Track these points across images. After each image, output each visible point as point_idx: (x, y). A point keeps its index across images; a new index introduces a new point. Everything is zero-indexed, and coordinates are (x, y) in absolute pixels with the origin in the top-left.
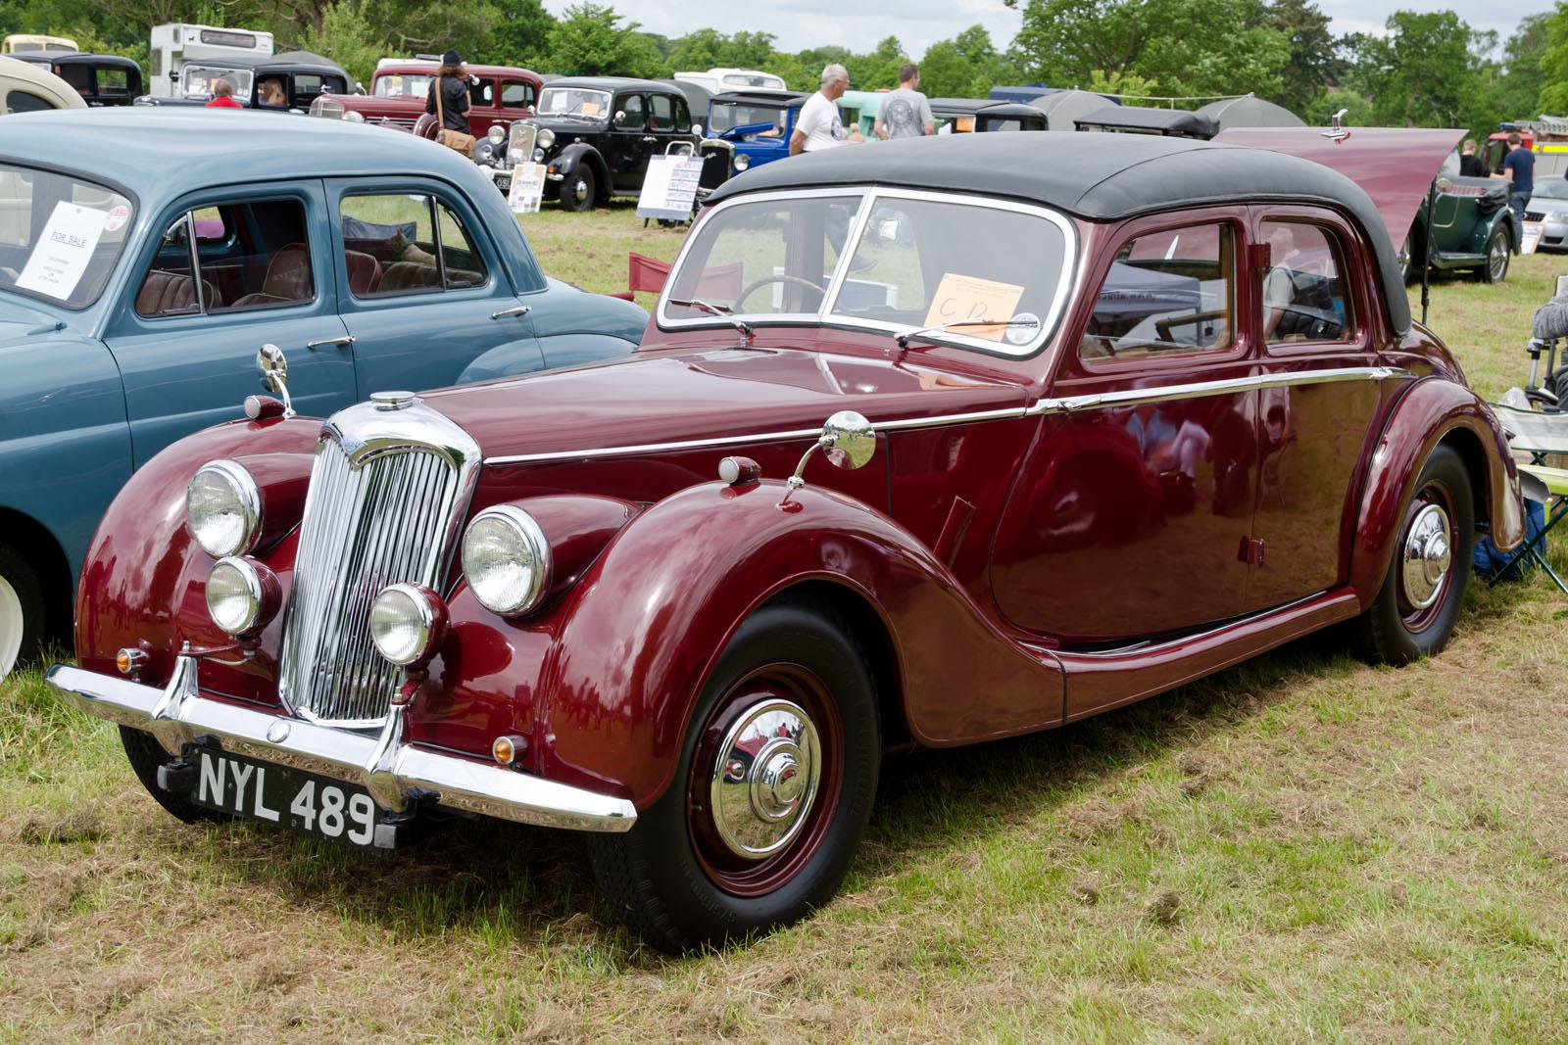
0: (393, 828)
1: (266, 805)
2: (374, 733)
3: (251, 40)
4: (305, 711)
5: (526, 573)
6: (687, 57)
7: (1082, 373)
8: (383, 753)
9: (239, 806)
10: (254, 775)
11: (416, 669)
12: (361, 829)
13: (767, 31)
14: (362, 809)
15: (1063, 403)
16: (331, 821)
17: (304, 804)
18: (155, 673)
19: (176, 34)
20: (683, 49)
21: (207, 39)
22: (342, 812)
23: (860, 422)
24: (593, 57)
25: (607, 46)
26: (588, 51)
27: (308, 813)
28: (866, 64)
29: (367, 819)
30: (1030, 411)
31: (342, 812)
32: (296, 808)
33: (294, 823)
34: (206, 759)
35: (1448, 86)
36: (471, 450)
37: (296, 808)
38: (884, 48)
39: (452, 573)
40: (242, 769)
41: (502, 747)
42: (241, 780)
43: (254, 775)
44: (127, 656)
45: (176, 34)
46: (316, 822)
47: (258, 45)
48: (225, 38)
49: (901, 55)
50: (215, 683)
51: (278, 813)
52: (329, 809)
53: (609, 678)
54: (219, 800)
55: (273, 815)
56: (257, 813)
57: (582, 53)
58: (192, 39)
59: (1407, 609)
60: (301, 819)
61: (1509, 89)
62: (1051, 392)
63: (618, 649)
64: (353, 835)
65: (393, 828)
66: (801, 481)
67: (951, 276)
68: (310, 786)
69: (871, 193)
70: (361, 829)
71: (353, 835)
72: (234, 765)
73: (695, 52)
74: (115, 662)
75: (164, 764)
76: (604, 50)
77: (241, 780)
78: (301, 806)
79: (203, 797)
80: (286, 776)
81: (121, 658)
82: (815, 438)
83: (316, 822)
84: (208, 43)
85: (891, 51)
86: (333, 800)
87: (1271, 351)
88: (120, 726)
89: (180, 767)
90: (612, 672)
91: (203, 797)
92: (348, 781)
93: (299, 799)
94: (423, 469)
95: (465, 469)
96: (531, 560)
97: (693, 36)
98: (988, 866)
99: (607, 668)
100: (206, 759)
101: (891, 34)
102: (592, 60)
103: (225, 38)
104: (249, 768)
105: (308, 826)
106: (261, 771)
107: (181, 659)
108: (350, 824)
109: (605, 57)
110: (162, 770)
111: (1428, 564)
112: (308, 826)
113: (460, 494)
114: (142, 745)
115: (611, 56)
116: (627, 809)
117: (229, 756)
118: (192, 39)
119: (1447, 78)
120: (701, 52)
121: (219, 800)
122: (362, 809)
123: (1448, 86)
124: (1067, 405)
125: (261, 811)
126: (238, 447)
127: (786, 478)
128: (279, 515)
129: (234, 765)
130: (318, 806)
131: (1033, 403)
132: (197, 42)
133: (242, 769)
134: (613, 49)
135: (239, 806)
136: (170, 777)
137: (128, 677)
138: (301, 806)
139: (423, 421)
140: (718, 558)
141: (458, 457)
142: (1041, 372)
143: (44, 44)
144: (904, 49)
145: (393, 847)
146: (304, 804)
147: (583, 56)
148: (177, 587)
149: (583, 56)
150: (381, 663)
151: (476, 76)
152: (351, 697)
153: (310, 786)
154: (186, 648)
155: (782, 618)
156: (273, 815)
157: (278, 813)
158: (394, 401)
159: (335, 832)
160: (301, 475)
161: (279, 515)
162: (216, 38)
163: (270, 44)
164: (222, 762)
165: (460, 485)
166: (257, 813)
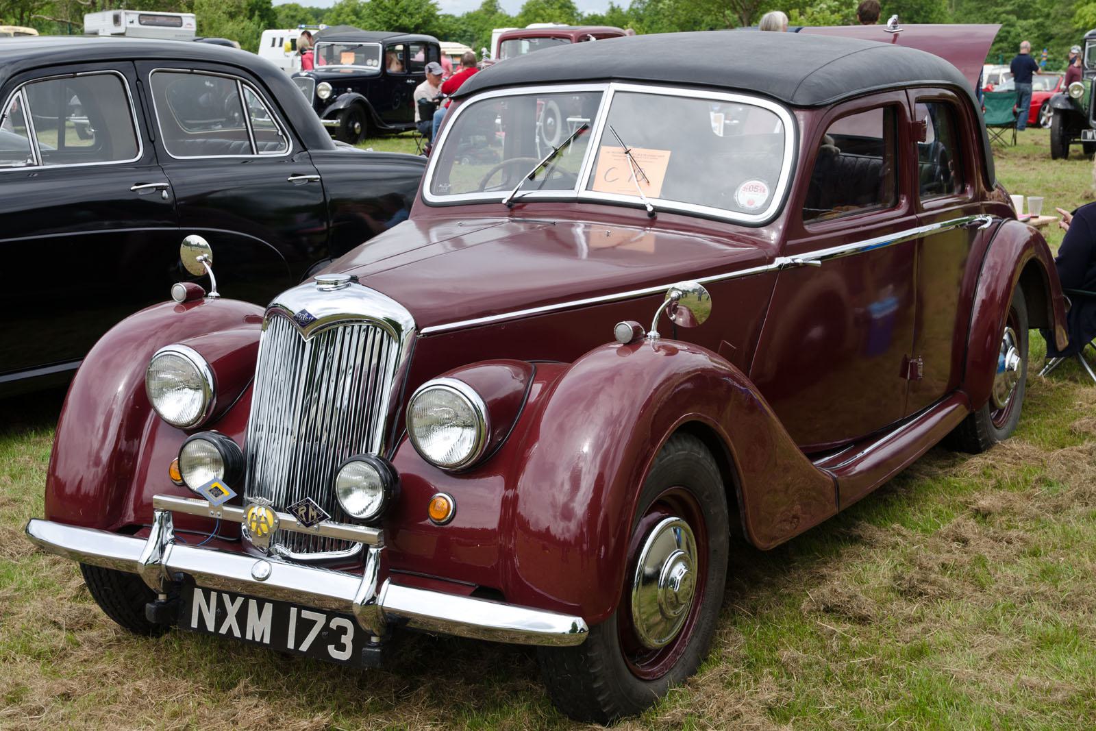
3: (178, 21)
6: (337, 20)
15: (793, 260)
19: (117, 20)
20: (334, 14)
21: (143, 22)
24: (405, 20)
25: (413, 11)
26: (399, 16)
28: (477, 19)
35: (923, 14)
36: (406, 319)
38: (486, 7)
45: (117, 20)
47: (184, 23)
48: (158, 20)
49: (500, 11)
51: (225, 633)
53: (91, 463)
57: (395, 18)
58: (132, 22)
61: (966, 14)
62: (784, 250)
63: (562, 484)
72: (226, 597)
73: (343, 16)
76: (411, 15)
84: (144, 24)
85: (492, 9)
90: (93, 458)
96: (197, 384)
97: (340, 4)
99: (89, 455)
102: (404, 23)
103: (158, 20)
104: (240, 600)
109: (414, 20)
111: (1008, 374)
113: (403, 358)
115: (418, 20)
118: (132, 22)
119: (922, 8)
120: (348, 16)
123: (923, 14)
124: (796, 261)
126: (173, 324)
128: (233, 377)
129: (226, 597)
131: (771, 261)
132: (136, 25)
134: (419, 13)
139: (360, 296)
140: (633, 403)
142: (773, 236)
143: (12, 32)
144: (501, 6)
147: (397, 21)
148: (738, 496)
149: (397, 21)
151: (593, 35)
155: (676, 455)
157: (225, 633)
160: (255, 340)
161: (233, 377)
162: (151, 20)
163: (193, 23)
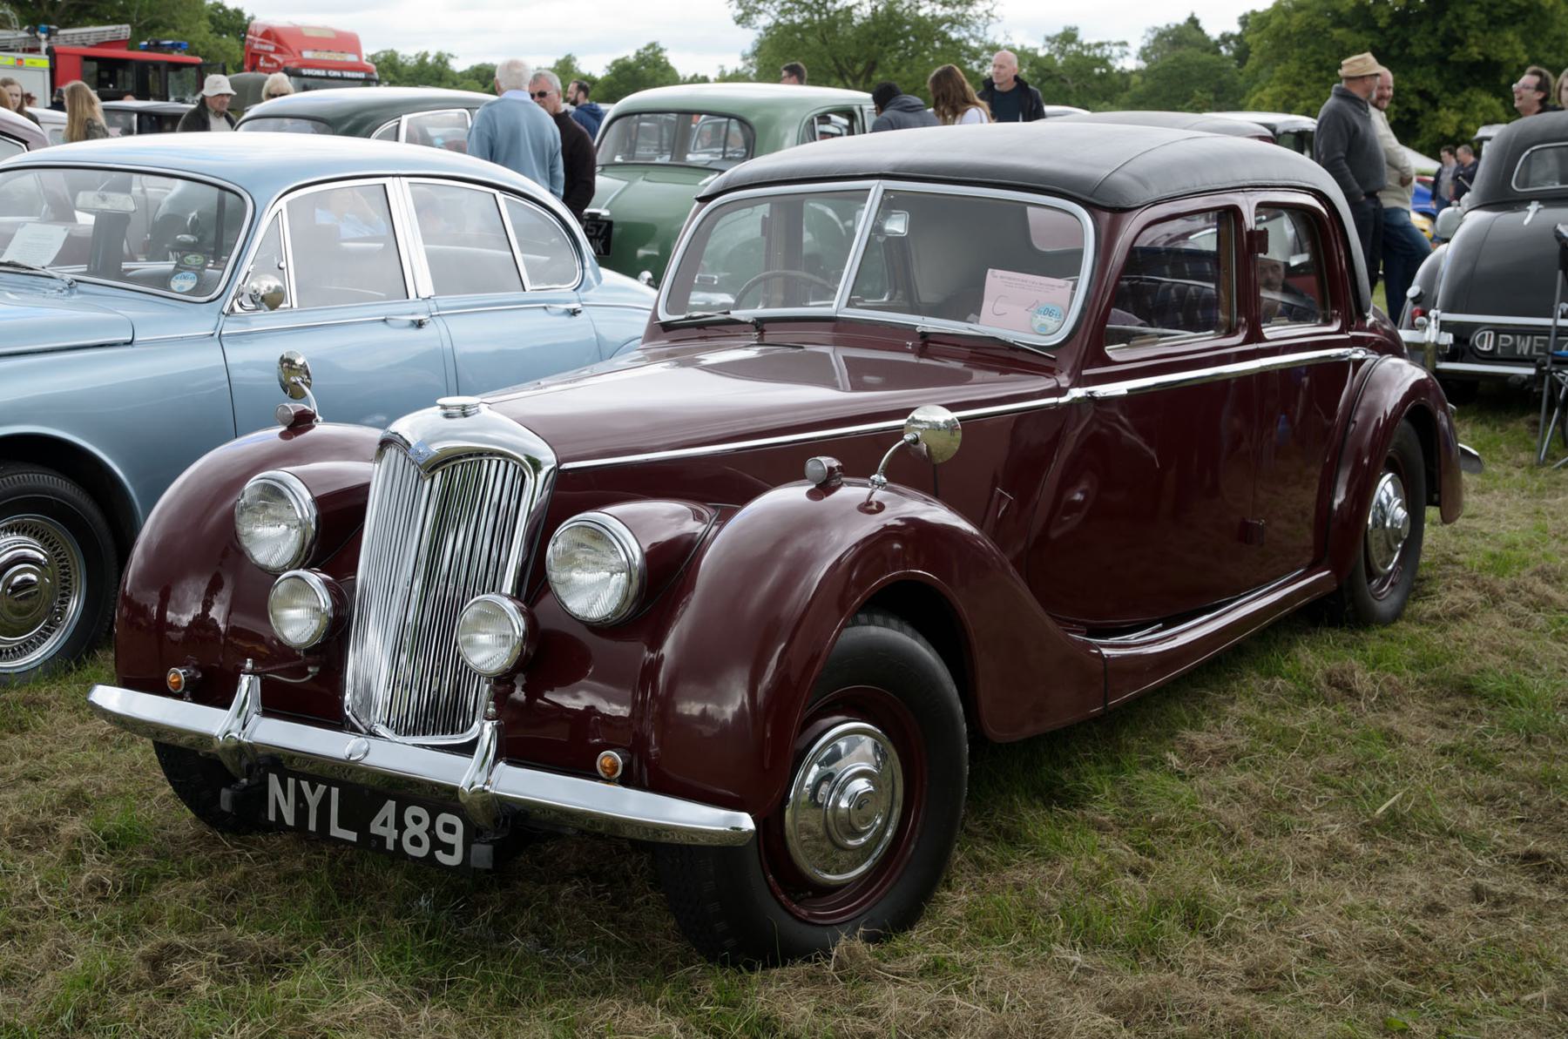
0: (490, 847)
1: (342, 824)
2: (468, 749)
4: (382, 730)
5: (295, 534)
7: (1108, 362)
8: (474, 770)
9: (312, 826)
10: (326, 799)
11: (502, 681)
12: (449, 849)
13: (446, 51)
14: (449, 828)
16: (416, 841)
17: (384, 824)
18: (214, 691)
22: (427, 832)
23: (943, 416)
27: (390, 834)
29: (457, 839)
30: (1063, 400)
31: (427, 832)
32: (376, 828)
33: (374, 843)
34: (273, 779)
37: (376, 828)
39: (534, 584)
40: (313, 789)
41: (607, 762)
42: (313, 800)
43: (327, 795)
44: (177, 675)
46: (398, 843)
50: (276, 704)
52: (412, 829)
54: (290, 820)
55: (352, 836)
56: (333, 833)
59: (1371, 574)
60: (382, 840)
64: (439, 854)
65: (490, 847)
66: (884, 479)
67: (999, 272)
68: (391, 806)
69: (876, 187)
70: (449, 849)
71: (439, 854)
72: (305, 785)
74: (164, 679)
75: (228, 787)
77: (313, 800)
78: (382, 825)
79: (272, 817)
80: (367, 792)
81: (171, 677)
82: (898, 433)
83: (398, 843)
86: (417, 820)
87: (1267, 336)
88: (155, 743)
89: (246, 788)
91: (272, 817)
92: (440, 798)
93: (379, 818)
94: (495, 479)
95: (541, 476)
98: (1076, 856)
100: (273, 779)
101: (1072, 24)
104: (321, 788)
105: (390, 846)
106: (335, 791)
107: (245, 680)
108: (436, 844)
110: (225, 793)
112: (390, 846)
114: (184, 759)
116: (746, 822)
117: (299, 776)
121: (290, 820)
122: (449, 828)
125: (336, 831)
127: (868, 477)
129: (305, 785)
130: (401, 826)
133: (313, 789)
135: (312, 826)
136: (235, 801)
137: (179, 697)
138: (382, 825)
141: (536, 465)
145: (490, 866)
146: (384, 824)
150: (465, 673)
152: (437, 716)
153: (391, 806)
154: (249, 665)
156: (352, 836)
158: (464, 407)
159: (421, 852)
160: (364, 481)
164: (291, 781)
165: (536, 490)
166: (333, 833)
